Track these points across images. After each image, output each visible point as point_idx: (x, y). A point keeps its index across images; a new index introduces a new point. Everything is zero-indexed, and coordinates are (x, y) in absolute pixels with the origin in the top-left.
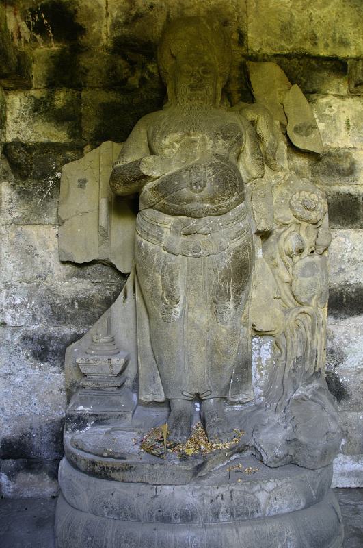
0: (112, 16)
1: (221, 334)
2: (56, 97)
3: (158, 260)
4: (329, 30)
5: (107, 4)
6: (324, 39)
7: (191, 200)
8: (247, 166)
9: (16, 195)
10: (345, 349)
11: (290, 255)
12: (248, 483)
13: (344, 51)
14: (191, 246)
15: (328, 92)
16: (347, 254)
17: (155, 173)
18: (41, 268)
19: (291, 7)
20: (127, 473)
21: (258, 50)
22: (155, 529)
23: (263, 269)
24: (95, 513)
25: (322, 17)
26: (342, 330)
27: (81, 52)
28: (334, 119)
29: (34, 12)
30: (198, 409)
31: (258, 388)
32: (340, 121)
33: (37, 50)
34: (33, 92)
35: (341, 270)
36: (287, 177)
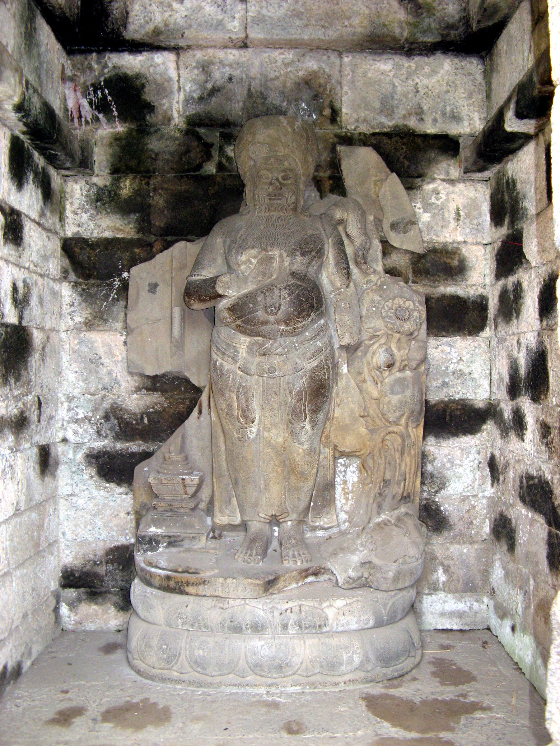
0: (185, 91)
1: (298, 454)
2: (122, 185)
3: (234, 380)
4: (438, 103)
5: (179, 77)
6: (432, 113)
7: (266, 323)
8: (328, 277)
9: (78, 298)
10: (448, 473)
11: (379, 368)
12: (318, 600)
13: (456, 126)
14: (266, 367)
15: (436, 176)
16: (452, 366)
17: (230, 292)
18: (106, 379)
19: (394, 76)
20: (201, 587)
21: (353, 127)
22: (227, 638)
23: (348, 386)
24: (170, 626)
25: (430, 87)
26: (445, 451)
27: (149, 134)
28: (442, 209)
29: (96, 87)
30: (276, 534)
31: (343, 513)
32: (449, 211)
33: (100, 132)
34: (95, 180)
35: (445, 384)
36: (379, 283)
